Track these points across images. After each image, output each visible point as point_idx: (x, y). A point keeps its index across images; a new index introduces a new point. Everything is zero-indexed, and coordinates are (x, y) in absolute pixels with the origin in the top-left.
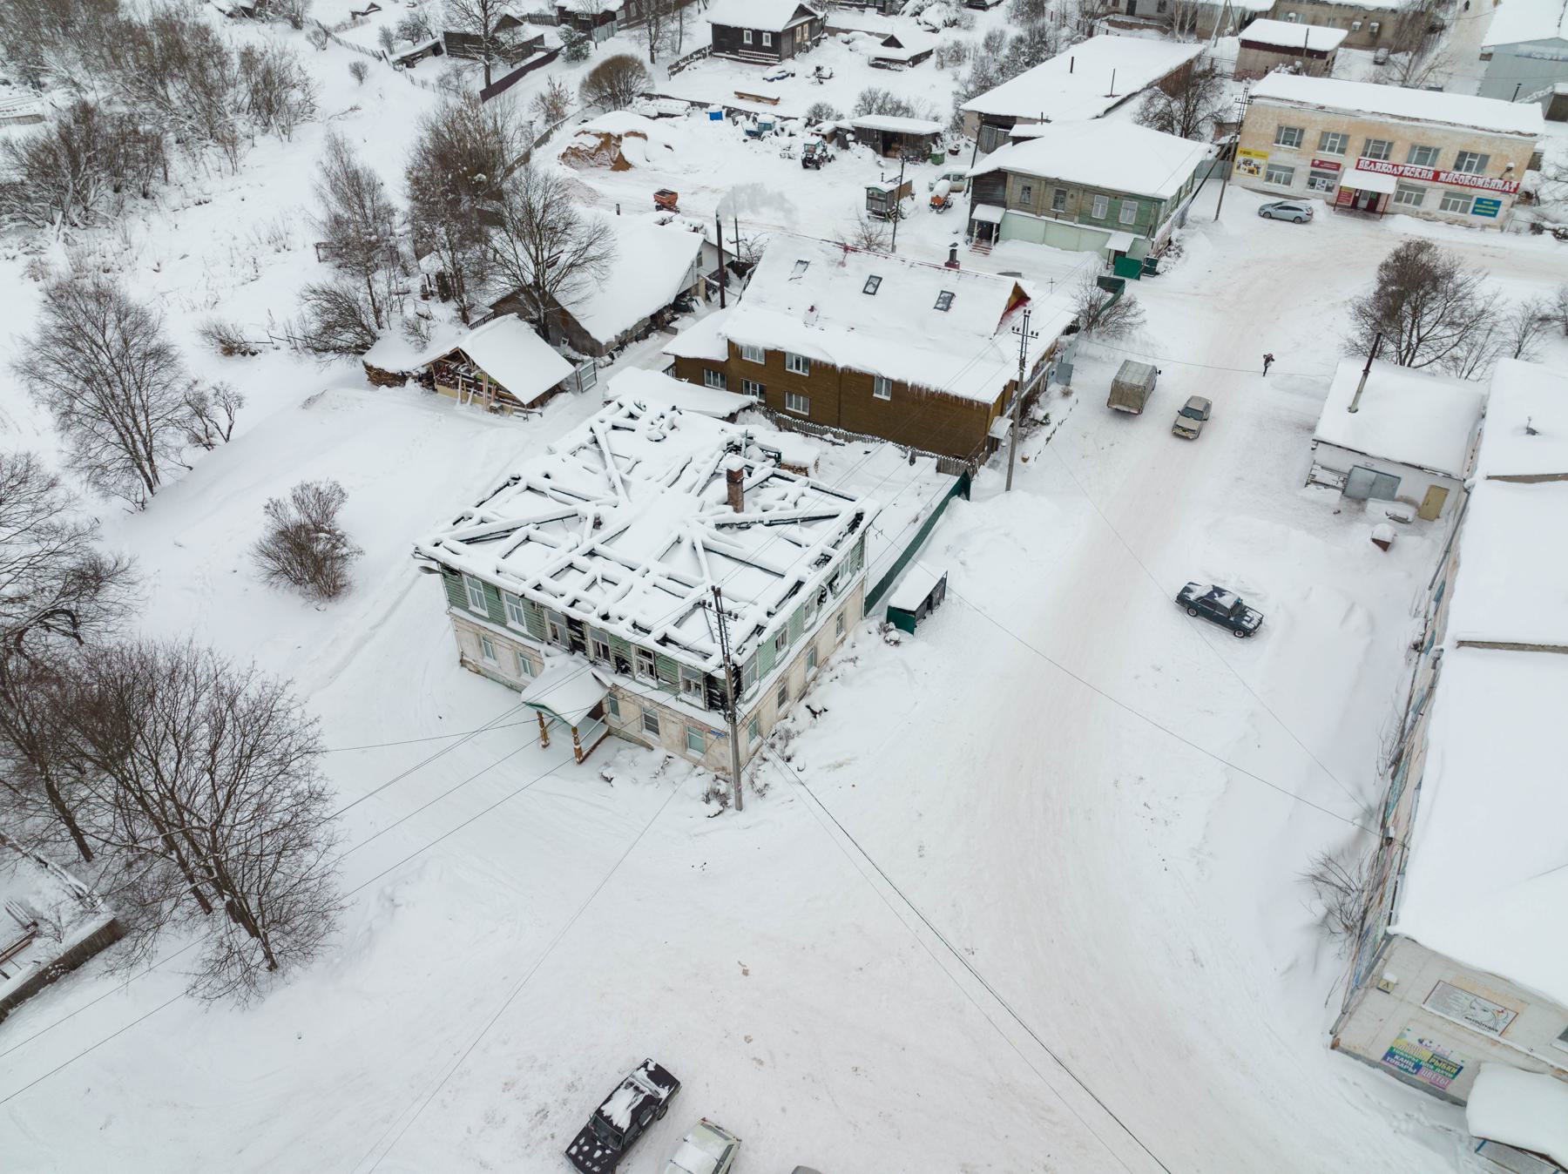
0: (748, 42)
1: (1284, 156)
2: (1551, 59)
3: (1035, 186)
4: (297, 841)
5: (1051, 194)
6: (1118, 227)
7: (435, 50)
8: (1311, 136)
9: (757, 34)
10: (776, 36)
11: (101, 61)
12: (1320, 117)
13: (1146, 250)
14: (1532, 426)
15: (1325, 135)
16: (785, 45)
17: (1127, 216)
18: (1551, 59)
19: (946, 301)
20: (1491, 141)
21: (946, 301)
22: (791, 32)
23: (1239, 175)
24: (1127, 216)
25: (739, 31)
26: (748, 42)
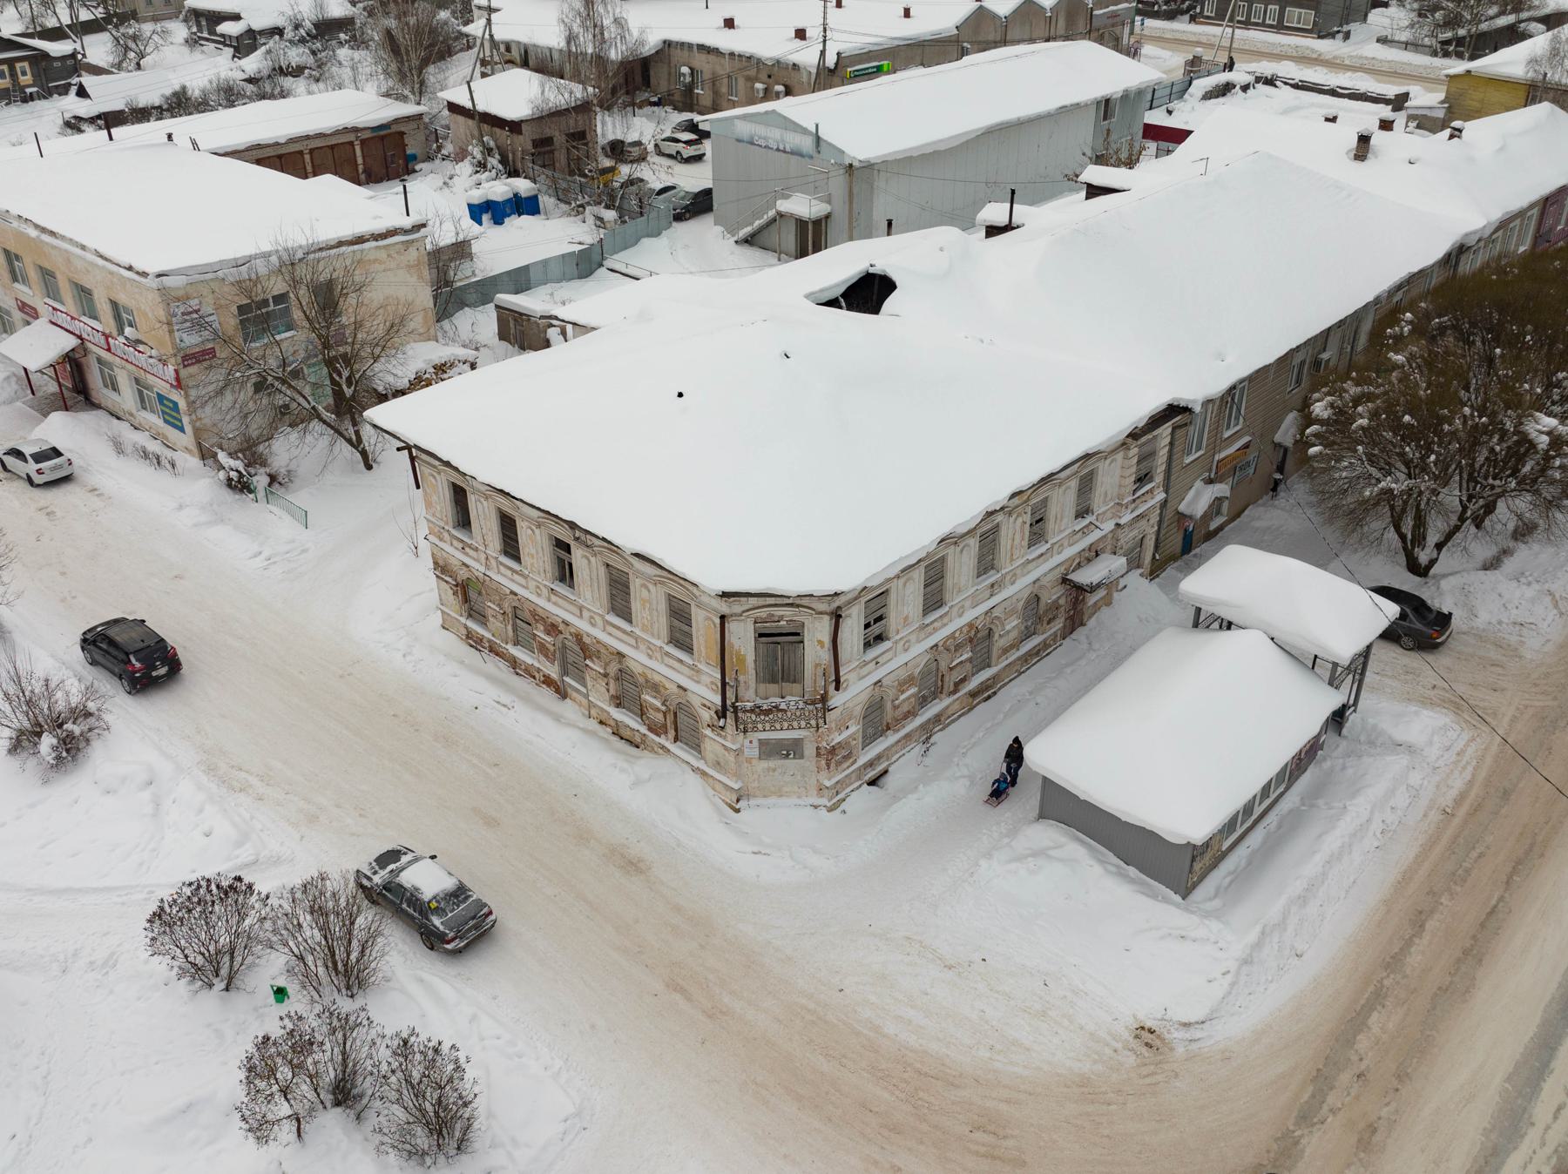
2: (778, 150)
18: (778, 150)
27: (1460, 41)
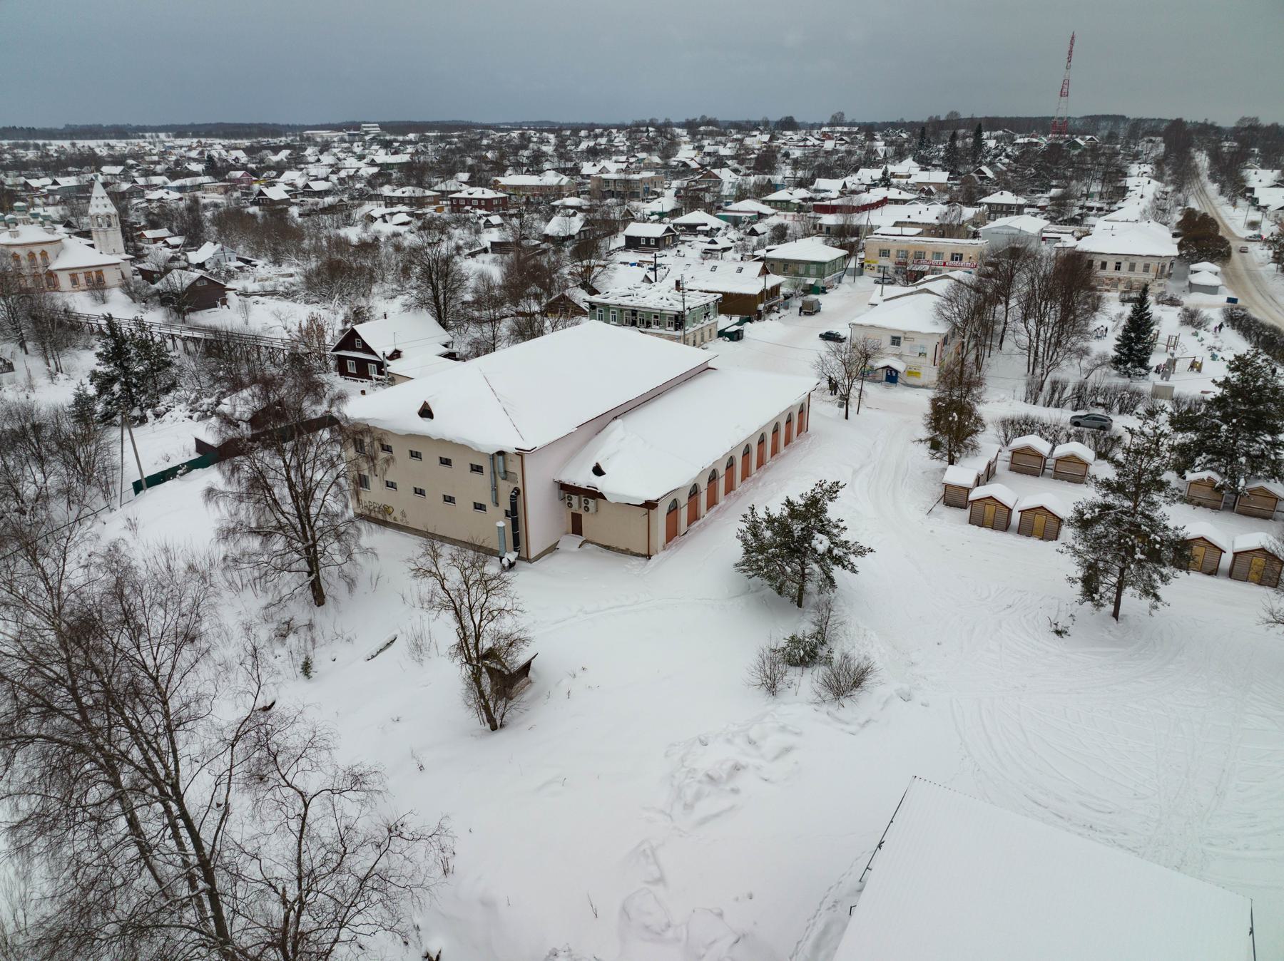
0: (643, 243)
1: (884, 261)
3: (775, 263)
4: (576, 224)
5: (782, 266)
6: (810, 276)
7: (485, 251)
8: (893, 252)
9: (648, 239)
10: (657, 240)
11: (71, 498)
12: (895, 244)
13: (821, 284)
14: (1060, 628)
15: (898, 251)
16: (661, 244)
17: (813, 270)
19: (740, 270)
20: (962, 248)
21: (740, 270)
22: (663, 239)
23: (866, 271)
24: (813, 270)
25: (639, 238)
26: (643, 243)
27: (1065, 221)
